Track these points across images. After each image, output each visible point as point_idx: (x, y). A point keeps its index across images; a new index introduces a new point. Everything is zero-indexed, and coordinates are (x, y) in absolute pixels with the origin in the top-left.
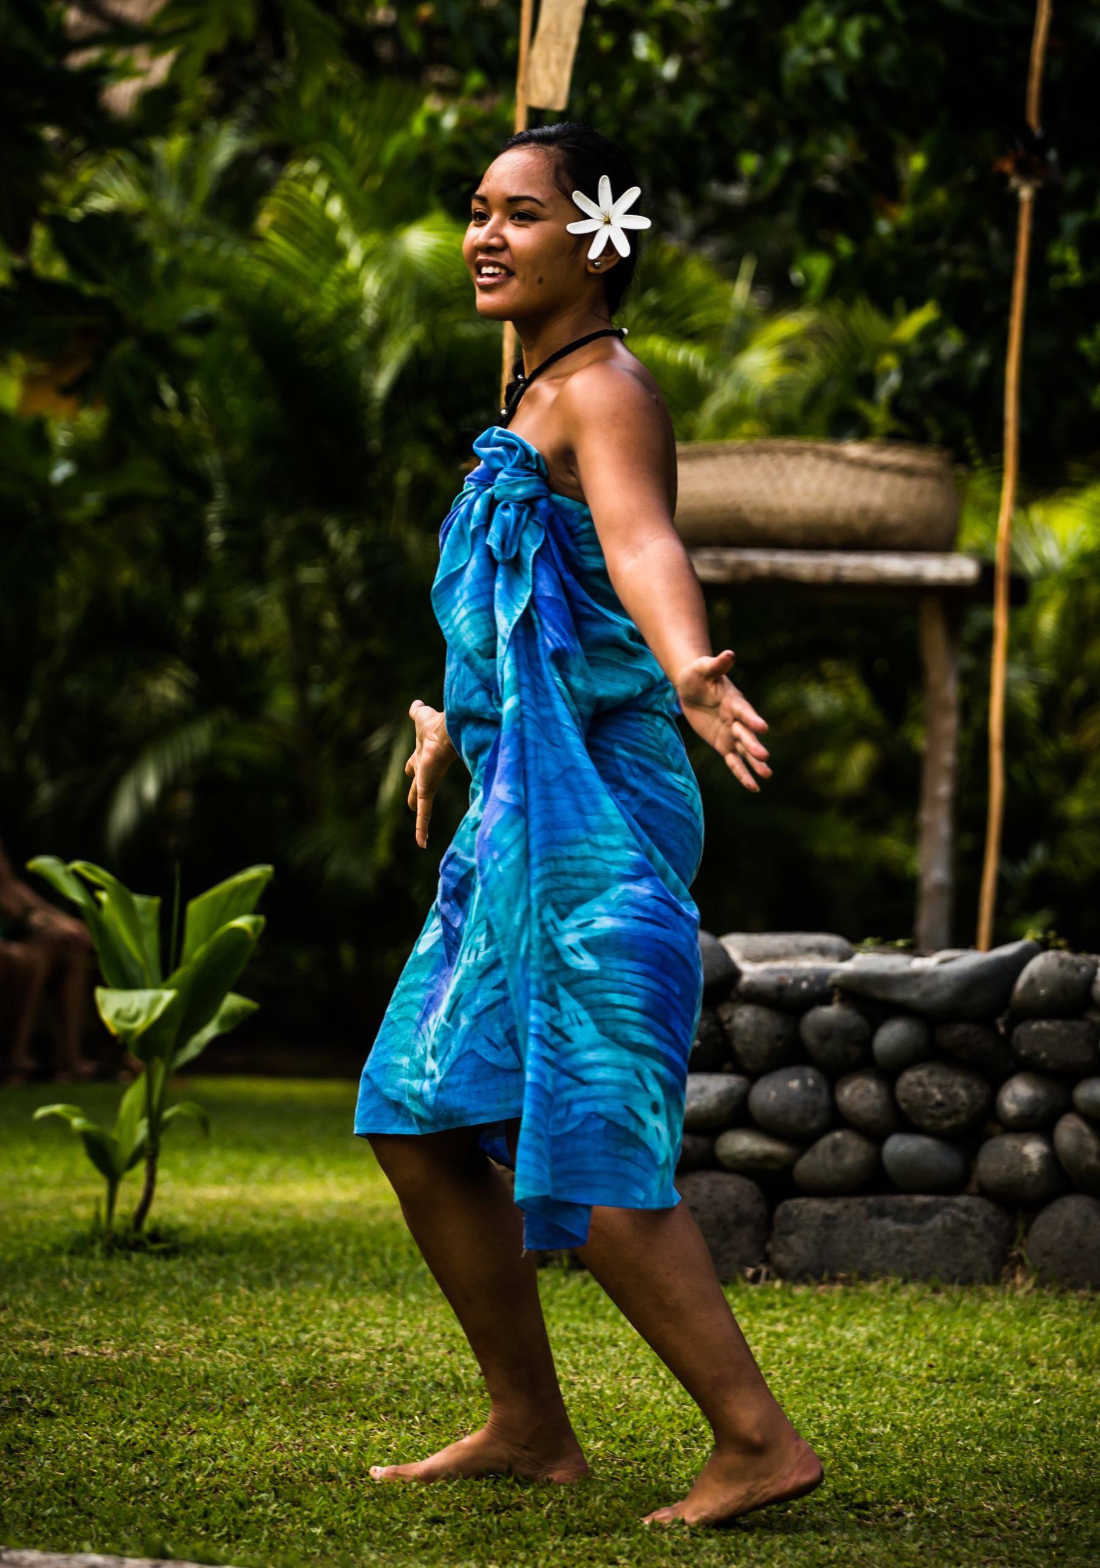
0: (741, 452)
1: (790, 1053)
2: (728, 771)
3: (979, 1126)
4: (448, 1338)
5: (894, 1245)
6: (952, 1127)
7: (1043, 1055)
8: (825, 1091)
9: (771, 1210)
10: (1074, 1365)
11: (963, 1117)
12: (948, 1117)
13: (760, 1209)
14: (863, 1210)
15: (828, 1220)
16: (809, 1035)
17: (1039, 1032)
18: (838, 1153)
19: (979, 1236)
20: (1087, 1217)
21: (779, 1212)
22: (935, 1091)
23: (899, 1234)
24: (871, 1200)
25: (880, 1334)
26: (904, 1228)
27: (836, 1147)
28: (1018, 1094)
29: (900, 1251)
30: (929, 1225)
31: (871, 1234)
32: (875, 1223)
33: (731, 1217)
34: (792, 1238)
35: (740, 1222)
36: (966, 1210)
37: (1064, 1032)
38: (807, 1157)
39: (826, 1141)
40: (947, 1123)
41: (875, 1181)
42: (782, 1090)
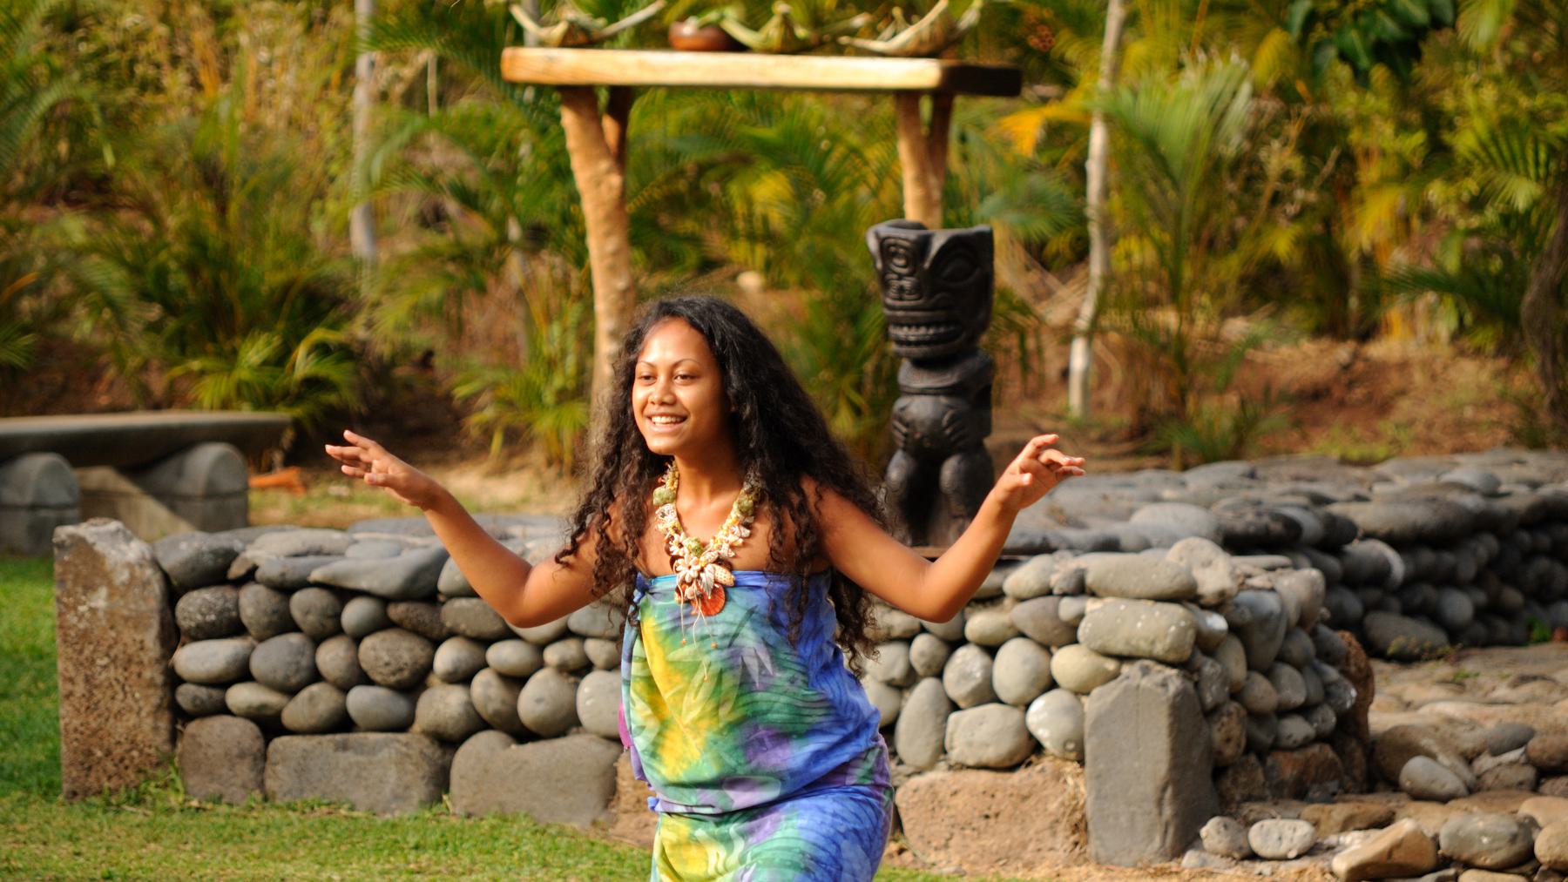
0: (645, 559)
1: (284, 624)
3: (413, 685)
4: (131, 775)
5: (354, 772)
8: (308, 652)
12: (394, 673)
13: (259, 744)
15: (306, 755)
16: (296, 613)
18: (315, 702)
19: (416, 764)
20: (493, 749)
23: (358, 763)
25: (664, 219)
27: (311, 698)
28: (447, 656)
29: (358, 776)
32: (341, 755)
33: (235, 751)
34: (279, 768)
35: (242, 756)
36: (406, 745)
42: (273, 656)
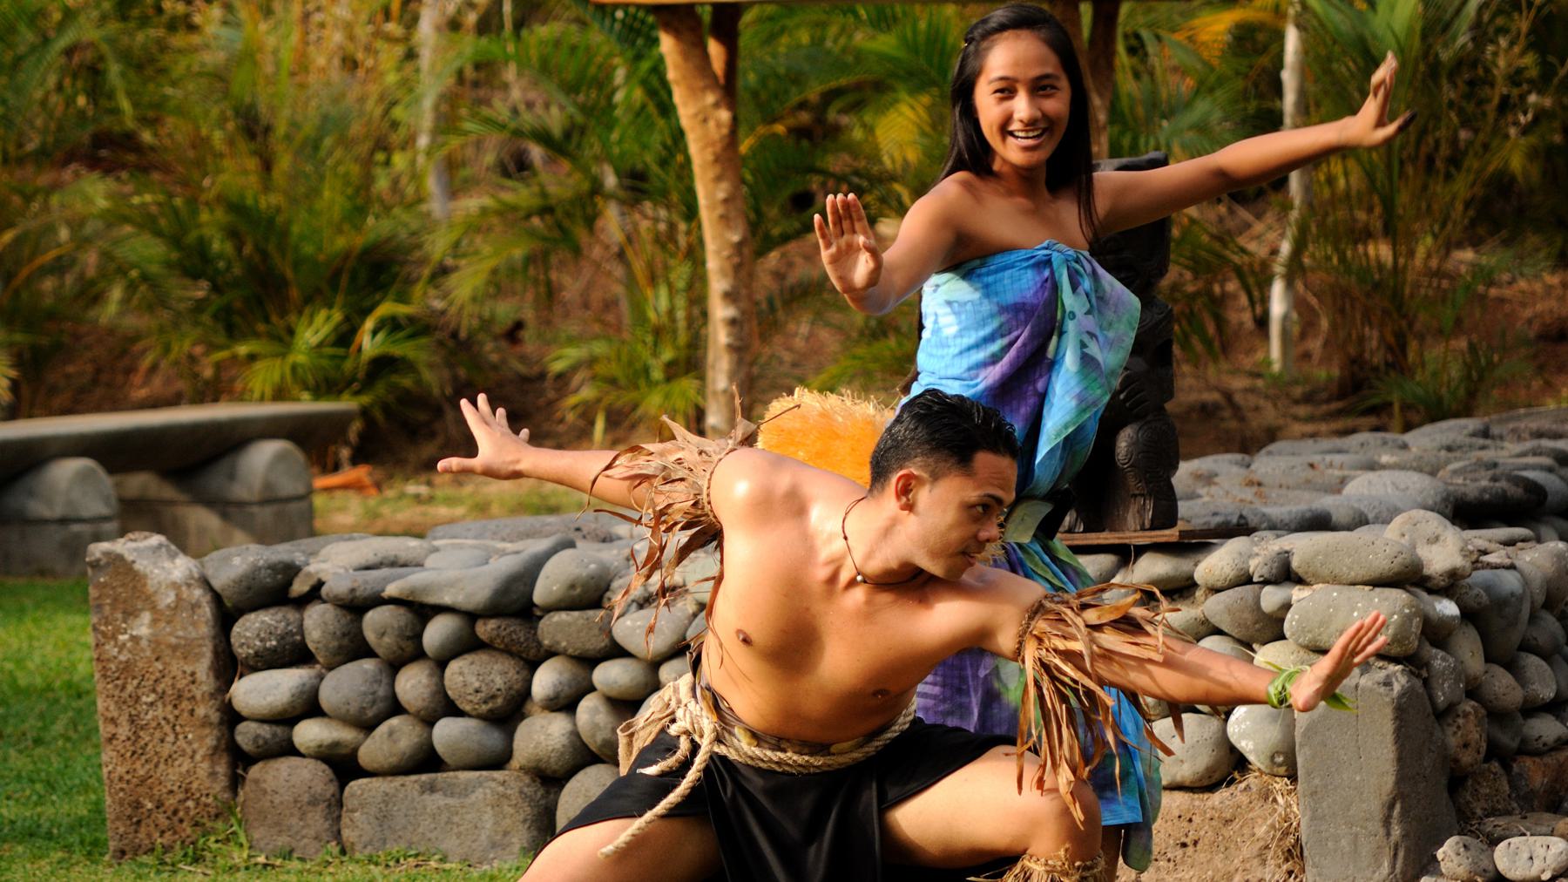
2: (1405, 864)
3: (508, 713)
5: (444, 818)
6: (491, 711)
7: (564, 644)
8: (385, 681)
9: (342, 788)
10: (641, 429)
11: (500, 701)
13: (333, 788)
14: (417, 786)
16: (370, 636)
17: (558, 624)
18: (391, 740)
21: (347, 789)
22: (473, 679)
24: (424, 777)
26: (451, 801)
28: (545, 680)
30: (473, 797)
31: (425, 808)
33: (306, 798)
37: (581, 622)
38: (369, 741)
39: (383, 728)
40: (484, 708)
41: (427, 761)
42: (346, 684)
